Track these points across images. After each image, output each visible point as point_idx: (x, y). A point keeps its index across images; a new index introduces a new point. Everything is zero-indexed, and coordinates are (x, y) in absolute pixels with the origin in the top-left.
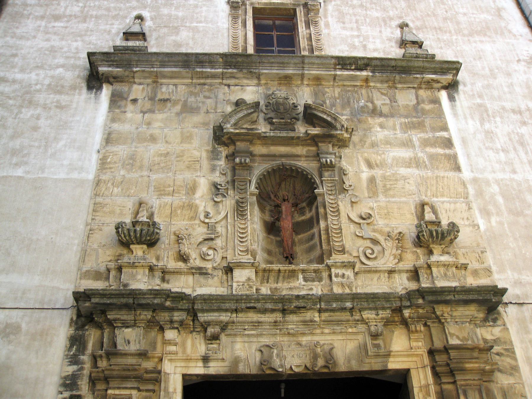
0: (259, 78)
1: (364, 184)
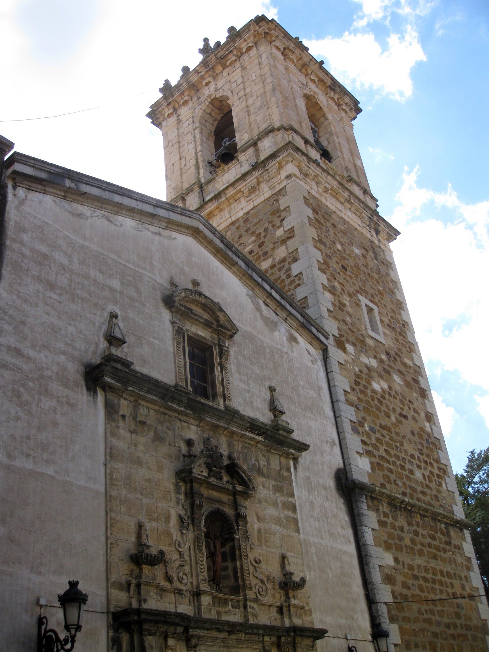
0: (200, 422)
1: (256, 532)
